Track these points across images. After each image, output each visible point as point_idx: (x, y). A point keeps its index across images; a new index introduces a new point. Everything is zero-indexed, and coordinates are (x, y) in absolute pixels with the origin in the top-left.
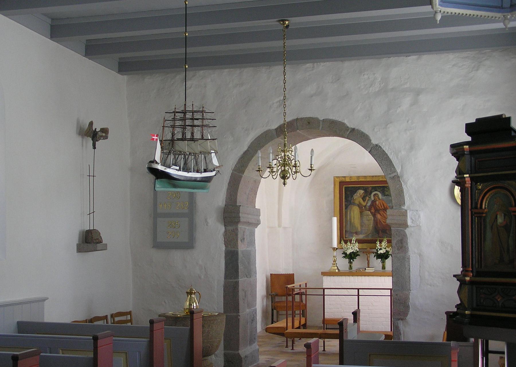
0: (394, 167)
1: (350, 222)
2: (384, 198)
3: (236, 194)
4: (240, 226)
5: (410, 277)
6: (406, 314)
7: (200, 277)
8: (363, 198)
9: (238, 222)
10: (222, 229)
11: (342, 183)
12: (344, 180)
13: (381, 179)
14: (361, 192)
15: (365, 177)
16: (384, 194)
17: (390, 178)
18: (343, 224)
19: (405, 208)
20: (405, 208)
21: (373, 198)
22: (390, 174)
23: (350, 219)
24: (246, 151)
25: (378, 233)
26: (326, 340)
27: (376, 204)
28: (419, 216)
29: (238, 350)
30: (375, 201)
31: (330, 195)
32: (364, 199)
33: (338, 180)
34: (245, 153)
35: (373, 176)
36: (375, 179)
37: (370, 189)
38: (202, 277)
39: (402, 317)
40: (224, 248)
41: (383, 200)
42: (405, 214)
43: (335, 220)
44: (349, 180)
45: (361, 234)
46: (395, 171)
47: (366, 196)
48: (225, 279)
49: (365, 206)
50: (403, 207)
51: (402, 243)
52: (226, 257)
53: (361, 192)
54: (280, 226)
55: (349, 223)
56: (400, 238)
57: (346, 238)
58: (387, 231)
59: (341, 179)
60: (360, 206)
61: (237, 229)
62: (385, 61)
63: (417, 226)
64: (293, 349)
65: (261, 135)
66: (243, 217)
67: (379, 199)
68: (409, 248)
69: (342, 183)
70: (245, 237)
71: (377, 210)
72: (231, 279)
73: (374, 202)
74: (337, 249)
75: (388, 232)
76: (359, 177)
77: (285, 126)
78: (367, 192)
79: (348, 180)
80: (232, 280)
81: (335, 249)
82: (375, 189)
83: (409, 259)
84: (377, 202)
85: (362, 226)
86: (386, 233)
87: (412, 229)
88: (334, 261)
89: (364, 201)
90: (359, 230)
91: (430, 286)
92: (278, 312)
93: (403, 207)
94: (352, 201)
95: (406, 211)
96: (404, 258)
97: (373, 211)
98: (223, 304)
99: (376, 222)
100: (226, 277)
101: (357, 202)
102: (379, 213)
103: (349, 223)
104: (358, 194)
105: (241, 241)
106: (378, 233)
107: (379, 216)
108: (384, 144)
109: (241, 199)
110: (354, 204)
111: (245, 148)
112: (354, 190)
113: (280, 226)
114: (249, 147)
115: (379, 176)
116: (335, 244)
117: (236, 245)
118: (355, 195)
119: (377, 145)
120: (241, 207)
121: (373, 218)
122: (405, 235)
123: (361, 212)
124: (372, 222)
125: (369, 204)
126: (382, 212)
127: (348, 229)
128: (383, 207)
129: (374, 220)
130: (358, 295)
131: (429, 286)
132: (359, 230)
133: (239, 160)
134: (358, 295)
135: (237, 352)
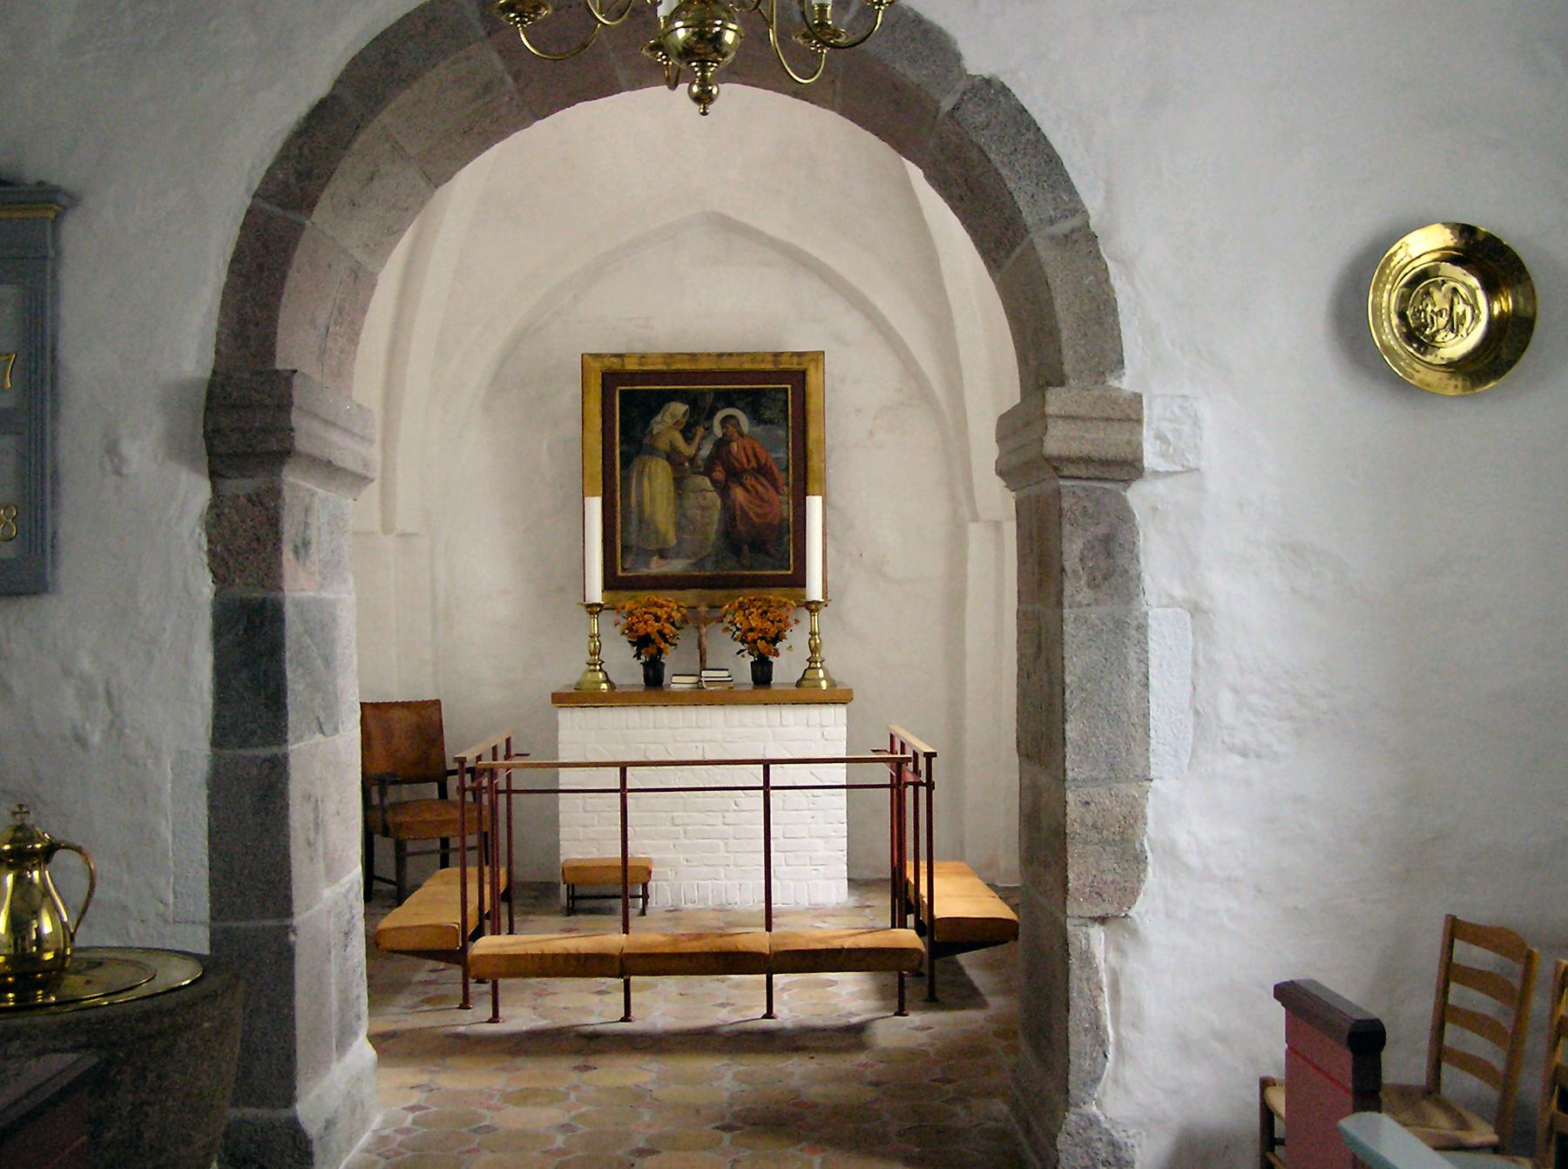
0: (1072, 190)
1: (641, 512)
2: (759, 429)
3: (272, 320)
4: (293, 480)
5: (1146, 716)
6: (1129, 893)
7: (81, 740)
8: (683, 432)
9: (283, 454)
10: (196, 491)
11: (611, 378)
12: (616, 364)
13: (747, 366)
14: (679, 409)
15: (693, 356)
16: (756, 417)
17: (1052, 237)
19: (1126, 383)
20: (1126, 383)
21: (718, 431)
22: (1052, 222)
23: (640, 504)
24: (322, 104)
26: (633, 979)
28: (1196, 423)
29: (289, 1100)
30: (729, 442)
31: (567, 421)
32: (687, 432)
33: (597, 366)
34: (322, 111)
35: (720, 355)
36: (727, 365)
37: (709, 399)
38: (96, 738)
39: (1110, 910)
40: (206, 588)
41: (751, 437)
42: (1129, 413)
43: (595, 505)
44: (636, 367)
45: (678, 555)
46: (1077, 209)
47: (696, 423)
48: (217, 742)
49: (692, 460)
50: (1113, 382)
51: (1109, 554)
52: (217, 634)
54: (387, 528)
55: (635, 521)
56: (1101, 530)
59: (607, 362)
60: (673, 457)
61: (277, 493)
63: (1190, 470)
64: (495, 1018)
65: (400, 22)
66: (307, 432)
67: (741, 435)
68: (1146, 577)
69: (611, 378)
70: (313, 534)
71: (734, 475)
72: (244, 744)
73: (722, 444)
75: (772, 551)
78: (700, 411)
79: (632, 366)
80: (249, 753)
82: (727, 399)
83: (1142, 628)
84: (734, 446)
85: (679, 527)
86: (767, 553)
87: (1160, 487)
89: (688, 439)
90: (672, 540)
91: (1244, 755)
92: (400, 847)
93: (1113, 382)
94: (646, 441)
95: (1138, 398)
96: (1120, 626)
97: (719, 474)
98: (204, 874)
99: (729, 513)
100: (221, 735)
101: (663, 444)
102: (742, 485)
103: (635, 521)
105: (296, 552)
107: (739, 494)
108: (1022, 75)
109: (295, 347)
110: (653, 451)
111: (320, 87)
113: (387, 528)
114: (339, 82)
115: (742, 354)
116: (596, 593)
117: (271, 575)
118: (658, 418)
119: (988, 82)
120: (297, 380)
121: (719, 503)
122: (1125, 516)
123: (679, 482)
124: (716, 515)
125: (706, 451)
126: (749, 481)
127: (633, 539)
128: (754, 464)
130: (766, 788)
131: (1238, 760)
132: (672, 540)
133: (287, 146)
134: (766, 788)
135: (284, 1114)
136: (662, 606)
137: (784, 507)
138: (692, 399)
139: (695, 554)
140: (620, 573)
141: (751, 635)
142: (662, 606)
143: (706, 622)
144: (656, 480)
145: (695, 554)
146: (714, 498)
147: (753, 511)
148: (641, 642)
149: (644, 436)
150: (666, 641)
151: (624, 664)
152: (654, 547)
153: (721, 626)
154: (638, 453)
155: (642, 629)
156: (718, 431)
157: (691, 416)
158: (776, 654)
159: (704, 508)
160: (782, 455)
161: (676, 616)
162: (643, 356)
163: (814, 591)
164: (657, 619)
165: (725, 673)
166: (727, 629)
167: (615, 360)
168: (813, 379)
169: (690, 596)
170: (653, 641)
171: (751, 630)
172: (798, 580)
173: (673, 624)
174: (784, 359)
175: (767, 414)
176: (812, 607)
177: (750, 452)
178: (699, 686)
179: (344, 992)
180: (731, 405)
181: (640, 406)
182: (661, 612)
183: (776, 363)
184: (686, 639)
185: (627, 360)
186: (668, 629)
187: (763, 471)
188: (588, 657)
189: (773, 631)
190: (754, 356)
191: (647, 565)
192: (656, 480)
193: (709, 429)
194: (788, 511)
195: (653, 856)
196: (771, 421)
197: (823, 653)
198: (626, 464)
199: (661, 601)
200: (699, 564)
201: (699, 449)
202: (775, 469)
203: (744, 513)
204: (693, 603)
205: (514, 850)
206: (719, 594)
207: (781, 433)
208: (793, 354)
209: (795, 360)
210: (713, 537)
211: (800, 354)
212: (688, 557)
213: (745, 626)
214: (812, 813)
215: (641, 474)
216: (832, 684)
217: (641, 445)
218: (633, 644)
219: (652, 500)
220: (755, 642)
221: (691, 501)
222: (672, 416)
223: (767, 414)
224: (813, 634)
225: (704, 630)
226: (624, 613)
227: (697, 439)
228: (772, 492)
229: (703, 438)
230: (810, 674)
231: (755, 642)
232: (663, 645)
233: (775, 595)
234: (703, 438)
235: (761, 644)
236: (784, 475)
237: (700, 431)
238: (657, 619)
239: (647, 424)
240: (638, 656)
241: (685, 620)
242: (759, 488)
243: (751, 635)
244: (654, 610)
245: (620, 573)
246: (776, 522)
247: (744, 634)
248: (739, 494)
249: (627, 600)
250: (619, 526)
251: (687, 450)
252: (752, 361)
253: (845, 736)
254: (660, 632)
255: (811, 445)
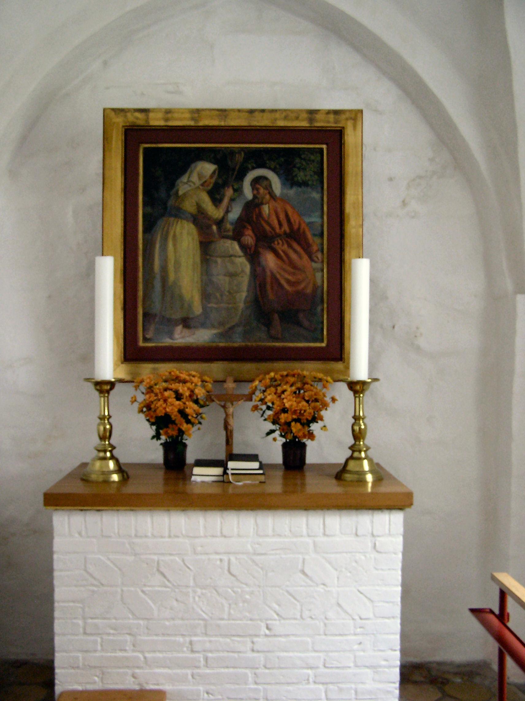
2: (292, 192)
13: (281, 123)
14: (207, 169)
15: (223, 113)
16: (290, 180)
18: (135, 307)
21: (248, 193)
25: (268, 324)
27: (260, 215)
33: (120, 121)
35: (251, 112)
37: (240, 158)
41: (284, 200)
43: (107, 269)
44: (162, 123)
45: (203, 325)
47: (225, 184)
49: (220, 223)
53: (207, 169)
57: (145, 340)
58: (301, 315)
59: (131, 118)
60: (199, 219)
62: (148, 462)
67: (273, 196)
71: (265, 239)
73: (252, 207)
74: (112, 384)
75: (306, 323)
76: (198, 111)
77: (120, 654)
78: (229, 172)
79: (156, 121)
81: (104, 388)
82: (259, 159)
84: (266, 209)
85: (206, 296)
86: (299, 324)
88: (102, 438)
90: (198, 309)
97: (249, 238)
99: (259, 277)
101: (189, 206)
102: (275, 252)
104: (195, 178)
106: (268, 324)
107: (270, 260)
110: (178, 213)
112: (182, 162)
118: (185, 178)
121: (248, 268)
123: (206, 246)
124: (245, 281)
125: (235, 214)
126: (281, 246)
127: (157, 307)
128: (286, 227)
129: (254, 275)
132: (198, 309)
136: (185, 382)
137: (318, 275)
138: (221, 159)
139: (221, 324)
140: (141, 344)
141: (283, 417)
142: (185, 382)
143: (233, 398)
144: (181, 243)
145: (221, 324)
146: (243, 264)
147: (285, 277)
148: (161, 422)
149: (169, 196)
150: (188, 422)
151: (140, 443)
152: (178, 316)
153: (251, 404)
154: (163, 215)
155: (161, 408)
156: (248, 193)
157: (220, 176)
158: (311, 436)
159: (232, 275)
160: (315, 219)
161: (200, 392)
162: (168, 111)
163: (360, 370)
164: (179, 396)
165: (256, 465)
166: (256, 408)
167: (138, 115)
168: (350, 138)
169: (217, 368)
170: (174, 422)
171: (284, 410)
172: (337, 351)
173: (196, 402)
174: (318, 116)
175: (301, 176)
176: (358, 388)
177: (282, 216)
178: (224, 480)
179: (295, 251)
180: (262, 165)
181: (158, 160)
182: (183, 389)
183: (311, 120)
184: (212, 415)
185: (151, 115)
186: (191, 408)
187: (295, 236)
188: (96, 441)
189: (309, 411)
190: (287, 113)
191: (171, 335)
192: (181, 243)
193: (238, 191)
194: (322, 278)
195: (167, 687)
196: (304, 184)
197: (369, 440)
198: (149, 228)
199: (184, 376)
200: (226, 334)
201: (227, 212)
202: (309, 235)
203: (274, 278)
204: (220, 377)
205: (363, 140)
206: (248, 367)
207: (316, 195)
208: (329, 112)
209: (332, 117)
210: (241, 305)
211: (336, 112)
212: (213, 327)
213: (277, 407)
214: (360, 638)
215: (165, 239)
216: (380, 475)
217: (166, 208)
218: (152, 424)
219: (177, 264)
220: (288, 424)
221: (219, 267)
222: (200, 176)
223: (301, 176)
224: (356, 418)
225: (231, 410)
226: (143, 388)
227: (226, 201)
228: (305, 257)
229: (232, 200)
230: (352, 465)
231: (288, 424)
232: (185, 427)
233: (309, 369)
234: (232, 200)
235: (296, 427)
236: (318, 240)
237: (229, 192)
238: (179, 396)
239: (172, 185)
240: (157, 436)
241: (210, 398)
242: (293, 256)
243: (283, 417)
244: (174, 386)
245: (141, 344)
246: (309, 291)
247: (277, 414)
248: (270, 260)
249: (147, 370)
250: (140, 294)
251: (215, 213)
252: (286, 118)
253: (400, 547)
254: (182, 413)
255: (349, 208)
